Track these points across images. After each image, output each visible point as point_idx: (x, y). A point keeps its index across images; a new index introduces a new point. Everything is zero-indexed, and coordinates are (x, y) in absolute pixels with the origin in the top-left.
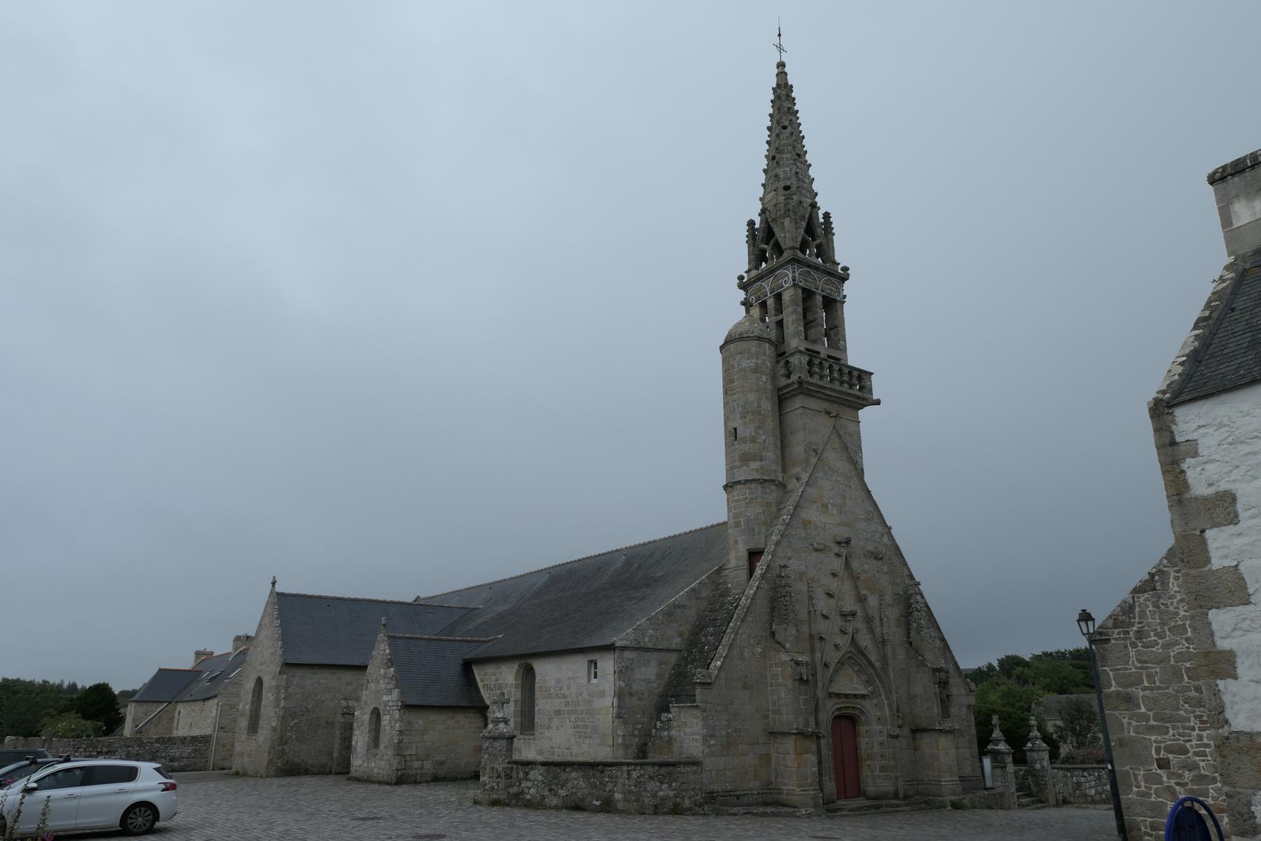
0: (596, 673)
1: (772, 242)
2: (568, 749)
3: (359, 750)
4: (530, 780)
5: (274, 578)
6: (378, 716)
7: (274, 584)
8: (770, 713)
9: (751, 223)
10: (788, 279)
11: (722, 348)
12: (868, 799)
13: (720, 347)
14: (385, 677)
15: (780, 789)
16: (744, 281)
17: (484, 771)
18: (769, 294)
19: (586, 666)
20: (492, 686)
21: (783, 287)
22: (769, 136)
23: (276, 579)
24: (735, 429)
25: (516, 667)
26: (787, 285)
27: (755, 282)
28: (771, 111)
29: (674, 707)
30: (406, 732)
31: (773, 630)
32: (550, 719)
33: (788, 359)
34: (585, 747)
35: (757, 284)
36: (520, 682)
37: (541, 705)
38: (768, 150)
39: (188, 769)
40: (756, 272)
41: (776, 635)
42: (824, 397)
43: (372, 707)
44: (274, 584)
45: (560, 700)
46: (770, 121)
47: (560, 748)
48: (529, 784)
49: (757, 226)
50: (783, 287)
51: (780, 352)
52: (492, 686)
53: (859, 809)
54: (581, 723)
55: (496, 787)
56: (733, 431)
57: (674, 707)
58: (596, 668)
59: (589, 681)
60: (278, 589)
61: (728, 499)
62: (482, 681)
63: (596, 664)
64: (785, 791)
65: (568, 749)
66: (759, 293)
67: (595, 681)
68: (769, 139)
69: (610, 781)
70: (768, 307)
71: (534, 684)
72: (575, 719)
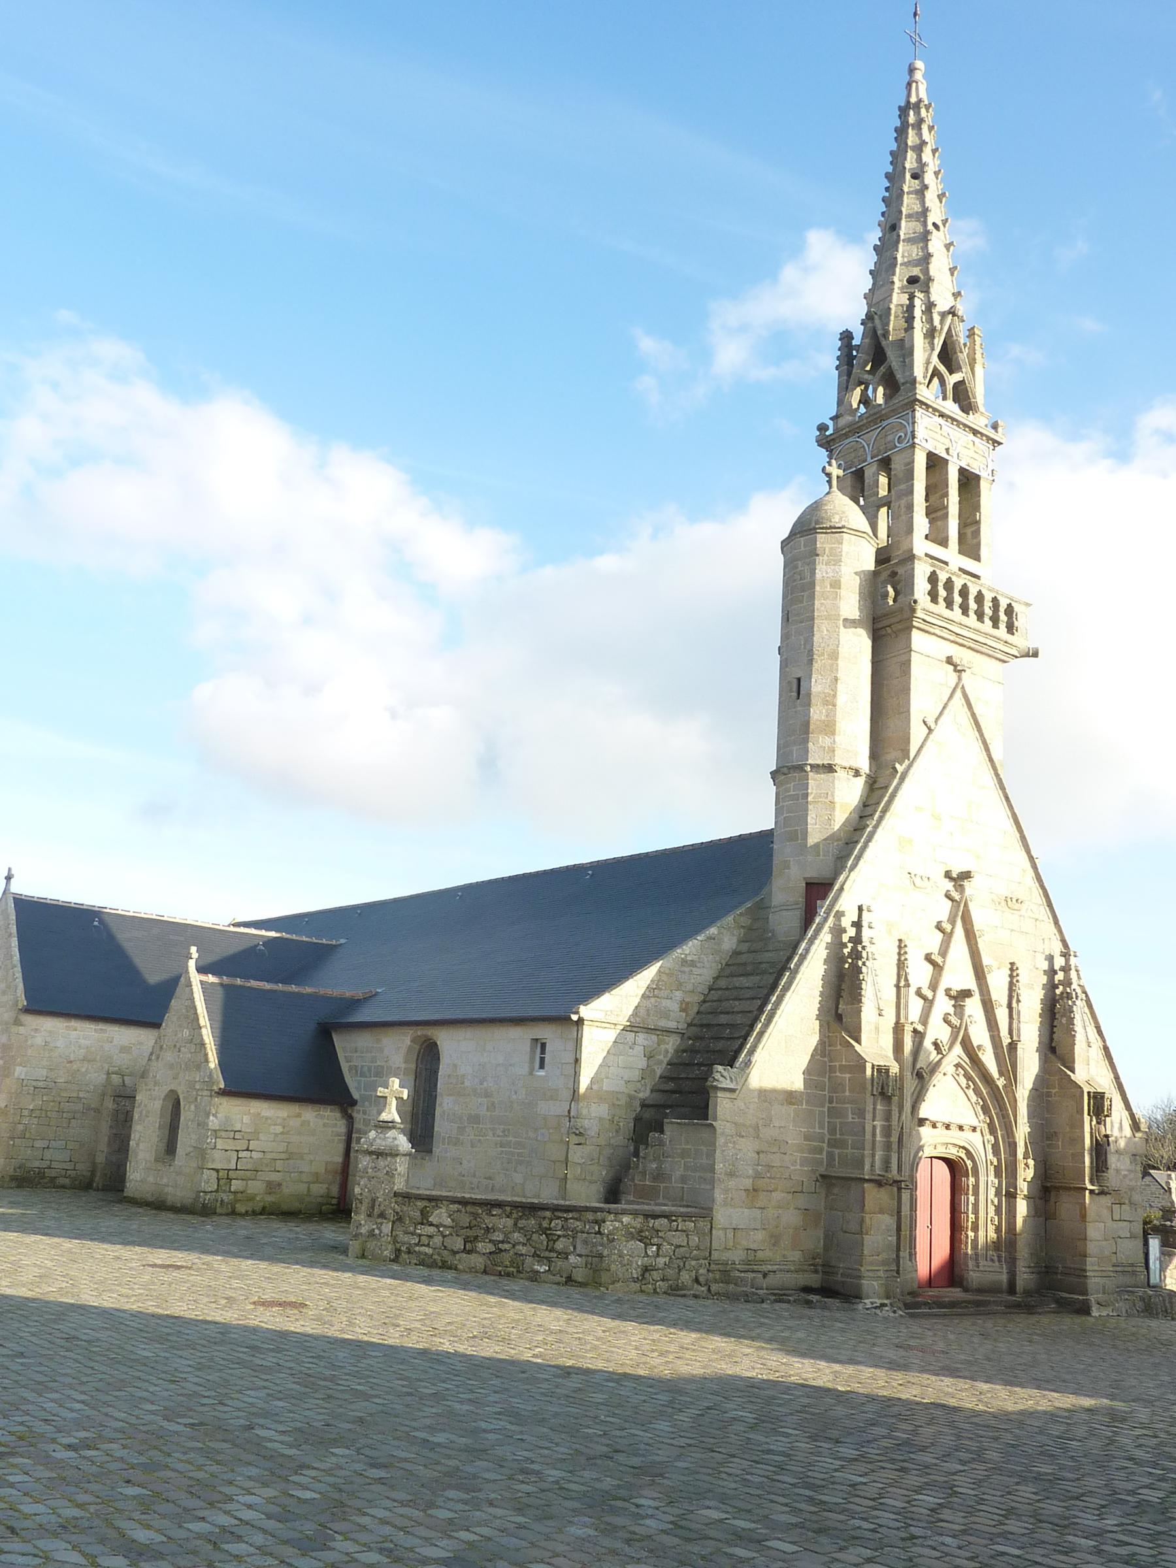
0: (542, 1060)
1: (882, 369)
2: (490, 1178)
3: (141, 1155)
4: (431, 1225)
5: (10, 869)
6: (177, 1105)
7: (9, 878)
8: (825, 1145)
9: (847, 336)
10: (906, 435)
11: (785, 544)
12: (966, 1290)
13: (782, 542)
14: (191, 1041)
15: (834, 1267)
16: (827, 433)
17: (359, 1205)
18: (869, 459)
19: (527, 1047)
20: (365, 1069)
21: (896, 447)
22: (887, 189)
23: (13, 872)
24: (799, 680)
25: (408, 1041)
26: (903, 445)
27: (846, 436)
28: (891, 159)
29: (672, 1123)
30: (223, 1134)
31: (839, 1012)
32: (461, 1130)
33: (896, 569)
34: (518, 1178)
35: (851, 439)
36: (413, 1066)
37: (445, 1104)
38: (883, 214)
39: (805, 1498)
40: (850, 418)
41: (844, 1020)
42: (952, 638)
43: (166, 1089)
44: (9, 878)
45: (480, 1100)
46: (891, 163)
47: (474, 1176)
48: (431, 1230)
49: (856, 341)
50: (896, 447)
51: (882, 557)
52: (365, 1069)
53: (953, 1305)
54: (514, 1139)
55: (377, 1232)
56: (795, 682)
57: (672, 1123)
58: (543, 1051)
59: (531, 1073)
60: (17, 888)
61: (777, 794)
62: (348, 1060)
63: (543, 1046)
64: (841, 1271)
65: (490, 1178)
66: (853, 455)
67: (542, 1073)
68: (887, 194)
69: (564, 1236)
70: (867, 481)
71: (436, 1072)
72: (503, 1132)
